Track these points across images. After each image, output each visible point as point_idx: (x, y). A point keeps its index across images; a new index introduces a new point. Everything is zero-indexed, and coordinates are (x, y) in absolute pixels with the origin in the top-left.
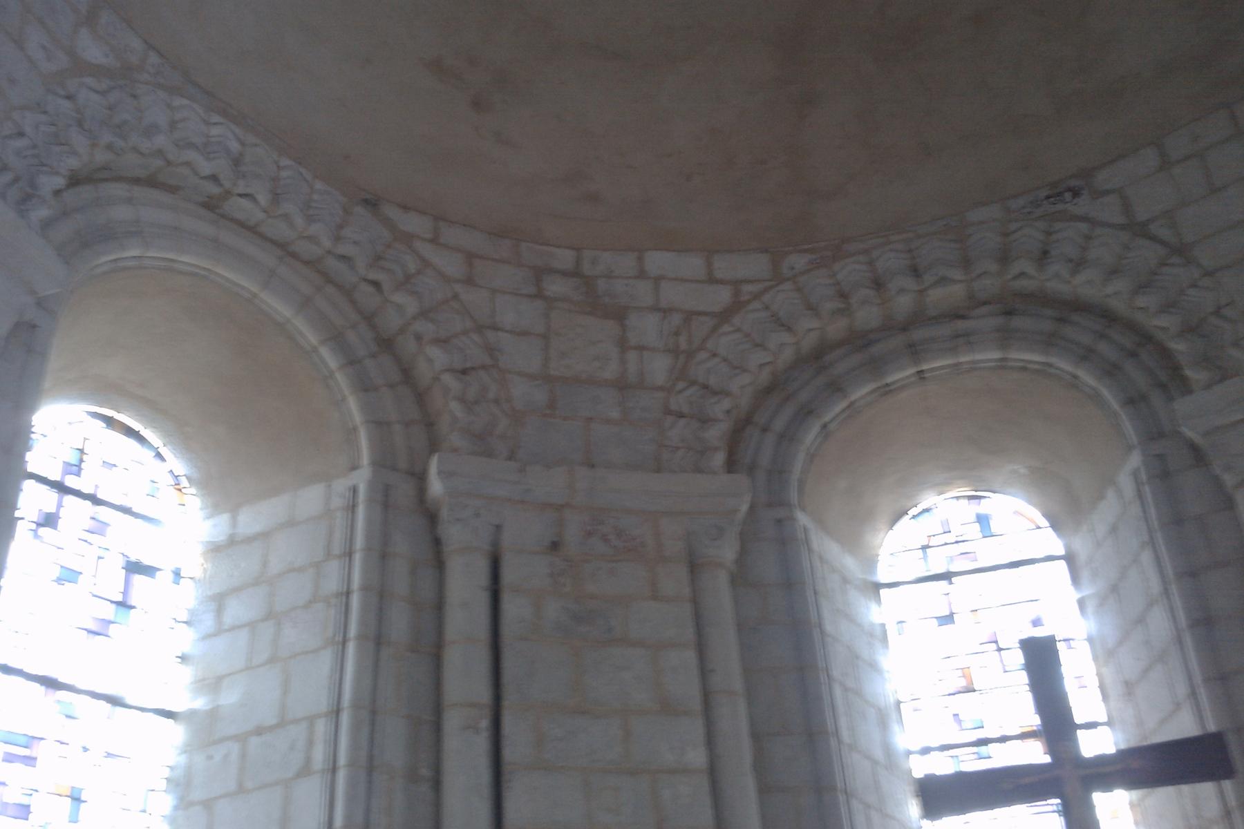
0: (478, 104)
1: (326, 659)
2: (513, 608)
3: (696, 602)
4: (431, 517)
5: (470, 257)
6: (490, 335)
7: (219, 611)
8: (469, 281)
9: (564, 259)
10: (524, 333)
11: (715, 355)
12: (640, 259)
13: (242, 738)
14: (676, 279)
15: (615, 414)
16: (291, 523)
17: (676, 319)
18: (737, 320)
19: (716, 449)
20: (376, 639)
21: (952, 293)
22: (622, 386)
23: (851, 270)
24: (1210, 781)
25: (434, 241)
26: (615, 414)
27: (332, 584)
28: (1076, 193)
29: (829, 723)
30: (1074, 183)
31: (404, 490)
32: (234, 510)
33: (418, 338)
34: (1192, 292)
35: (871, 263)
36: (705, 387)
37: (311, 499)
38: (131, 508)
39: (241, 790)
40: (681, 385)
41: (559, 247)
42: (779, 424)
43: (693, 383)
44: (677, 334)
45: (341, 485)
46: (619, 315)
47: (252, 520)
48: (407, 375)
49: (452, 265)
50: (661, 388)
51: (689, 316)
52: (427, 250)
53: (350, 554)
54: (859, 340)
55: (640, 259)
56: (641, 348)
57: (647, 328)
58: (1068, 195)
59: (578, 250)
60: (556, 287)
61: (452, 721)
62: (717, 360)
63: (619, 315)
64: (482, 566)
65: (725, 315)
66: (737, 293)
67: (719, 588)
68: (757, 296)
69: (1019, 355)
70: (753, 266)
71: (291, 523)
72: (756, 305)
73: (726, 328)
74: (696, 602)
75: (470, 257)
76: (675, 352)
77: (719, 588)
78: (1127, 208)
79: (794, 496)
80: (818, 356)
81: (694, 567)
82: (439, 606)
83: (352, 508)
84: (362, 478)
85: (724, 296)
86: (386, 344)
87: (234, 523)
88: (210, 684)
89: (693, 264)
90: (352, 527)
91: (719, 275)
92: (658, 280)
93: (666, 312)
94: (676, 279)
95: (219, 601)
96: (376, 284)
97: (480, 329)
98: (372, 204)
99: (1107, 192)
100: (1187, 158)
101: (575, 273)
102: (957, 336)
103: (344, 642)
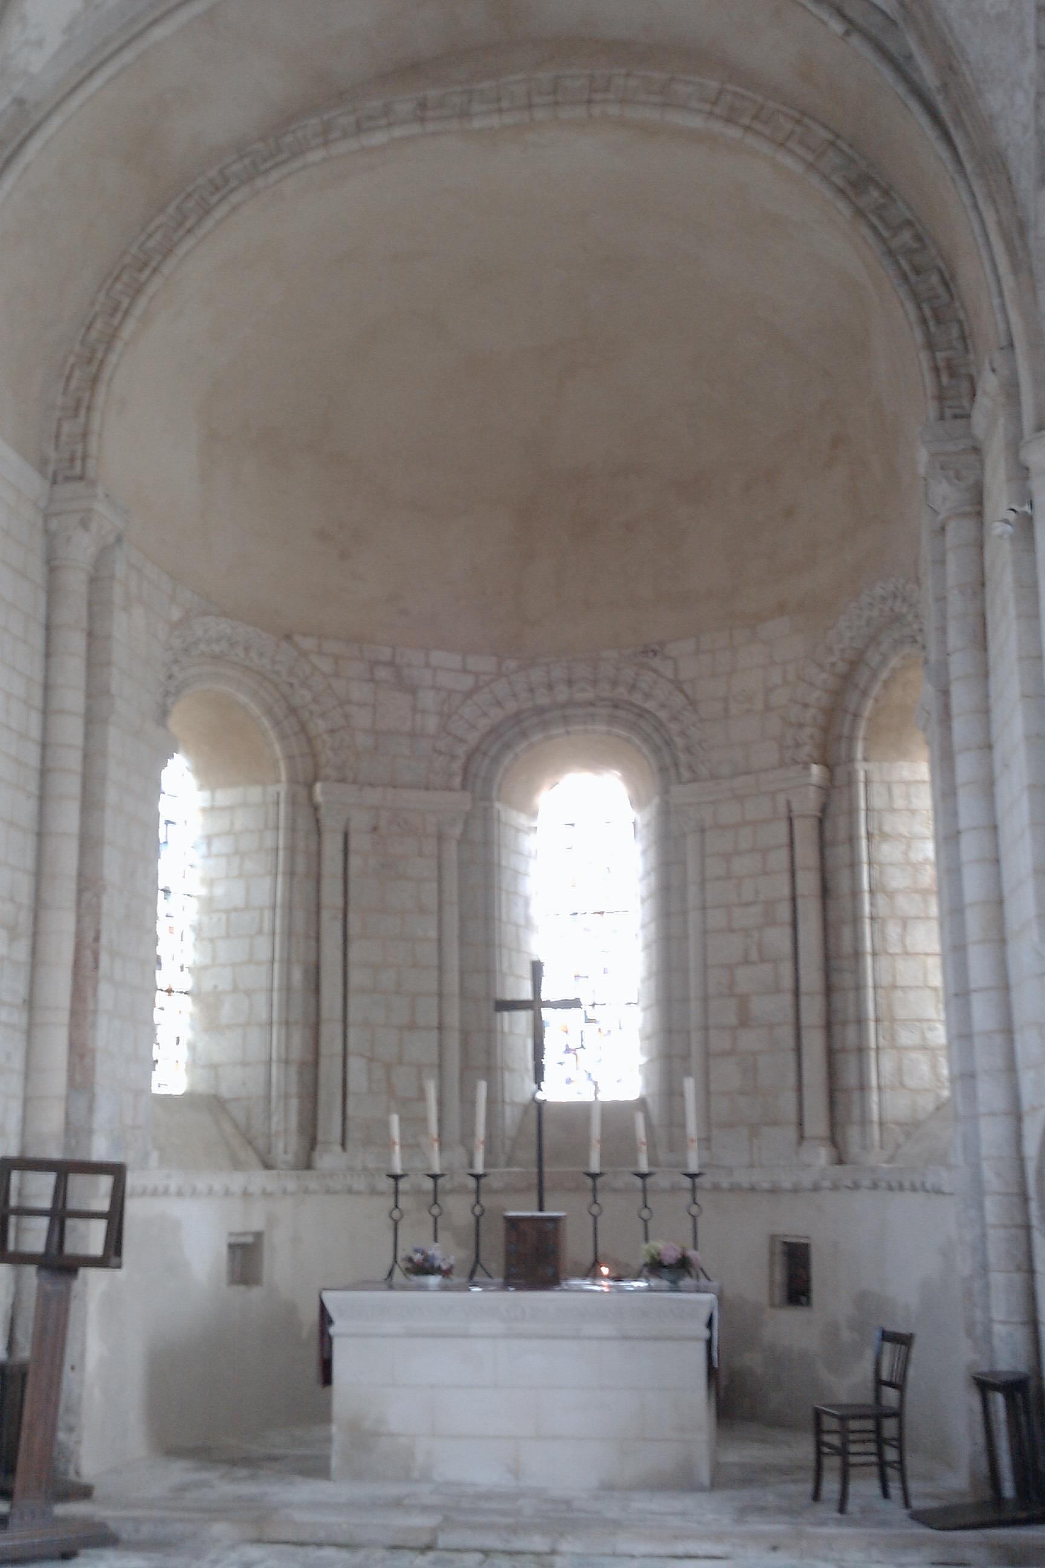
1: (267, 882)
2: (355, 862)
3: (439, 857)
4: (316, 808)
7: (209, 845)
8: (337, 675)
9: (386, 653)
13: (227, 912)
16: (245, 805)
20: (291, 874)
21: (589, 695)
23: (537, 675)
24: (5, 1263)
27: (269, 842)
28: (655, 652)
30: (657, 648)
31: (302, 793)
32: (213, 791)
33: (311, 712)
37: (255, 793)
39: (228, 936)
43: (449, 734)
45: (272, 790)
46: (413, 691)
47: (224, 797)
48: (303, 727)
49: (326, 665)
53: (277, 828)
54: (540, 711)
57: (428, 699)
60: (382, 673)
61: (326, 915)
63: (413, 691)
64: (340, 839)
65: (469, 694)
67: (452, 852)
69: (617, 730)
70: (485, 664)
71: (245, 805)
73: (469, 702)
74: (439, 857)
77: (452, 852)
78: (676, 670)
79: (494, 794)
80: (517, 717)
82: (319, 854)
84: (282, 788)
85: (468, 682)
86: (293, 711)
87: (213, 798)
88: (210, 883)
90: (278, 814)
95: (209, 839)
96: (291, 685)
98: (288, 637)
99: (670, 658)
101: (391, 664)
103: (276, 874)
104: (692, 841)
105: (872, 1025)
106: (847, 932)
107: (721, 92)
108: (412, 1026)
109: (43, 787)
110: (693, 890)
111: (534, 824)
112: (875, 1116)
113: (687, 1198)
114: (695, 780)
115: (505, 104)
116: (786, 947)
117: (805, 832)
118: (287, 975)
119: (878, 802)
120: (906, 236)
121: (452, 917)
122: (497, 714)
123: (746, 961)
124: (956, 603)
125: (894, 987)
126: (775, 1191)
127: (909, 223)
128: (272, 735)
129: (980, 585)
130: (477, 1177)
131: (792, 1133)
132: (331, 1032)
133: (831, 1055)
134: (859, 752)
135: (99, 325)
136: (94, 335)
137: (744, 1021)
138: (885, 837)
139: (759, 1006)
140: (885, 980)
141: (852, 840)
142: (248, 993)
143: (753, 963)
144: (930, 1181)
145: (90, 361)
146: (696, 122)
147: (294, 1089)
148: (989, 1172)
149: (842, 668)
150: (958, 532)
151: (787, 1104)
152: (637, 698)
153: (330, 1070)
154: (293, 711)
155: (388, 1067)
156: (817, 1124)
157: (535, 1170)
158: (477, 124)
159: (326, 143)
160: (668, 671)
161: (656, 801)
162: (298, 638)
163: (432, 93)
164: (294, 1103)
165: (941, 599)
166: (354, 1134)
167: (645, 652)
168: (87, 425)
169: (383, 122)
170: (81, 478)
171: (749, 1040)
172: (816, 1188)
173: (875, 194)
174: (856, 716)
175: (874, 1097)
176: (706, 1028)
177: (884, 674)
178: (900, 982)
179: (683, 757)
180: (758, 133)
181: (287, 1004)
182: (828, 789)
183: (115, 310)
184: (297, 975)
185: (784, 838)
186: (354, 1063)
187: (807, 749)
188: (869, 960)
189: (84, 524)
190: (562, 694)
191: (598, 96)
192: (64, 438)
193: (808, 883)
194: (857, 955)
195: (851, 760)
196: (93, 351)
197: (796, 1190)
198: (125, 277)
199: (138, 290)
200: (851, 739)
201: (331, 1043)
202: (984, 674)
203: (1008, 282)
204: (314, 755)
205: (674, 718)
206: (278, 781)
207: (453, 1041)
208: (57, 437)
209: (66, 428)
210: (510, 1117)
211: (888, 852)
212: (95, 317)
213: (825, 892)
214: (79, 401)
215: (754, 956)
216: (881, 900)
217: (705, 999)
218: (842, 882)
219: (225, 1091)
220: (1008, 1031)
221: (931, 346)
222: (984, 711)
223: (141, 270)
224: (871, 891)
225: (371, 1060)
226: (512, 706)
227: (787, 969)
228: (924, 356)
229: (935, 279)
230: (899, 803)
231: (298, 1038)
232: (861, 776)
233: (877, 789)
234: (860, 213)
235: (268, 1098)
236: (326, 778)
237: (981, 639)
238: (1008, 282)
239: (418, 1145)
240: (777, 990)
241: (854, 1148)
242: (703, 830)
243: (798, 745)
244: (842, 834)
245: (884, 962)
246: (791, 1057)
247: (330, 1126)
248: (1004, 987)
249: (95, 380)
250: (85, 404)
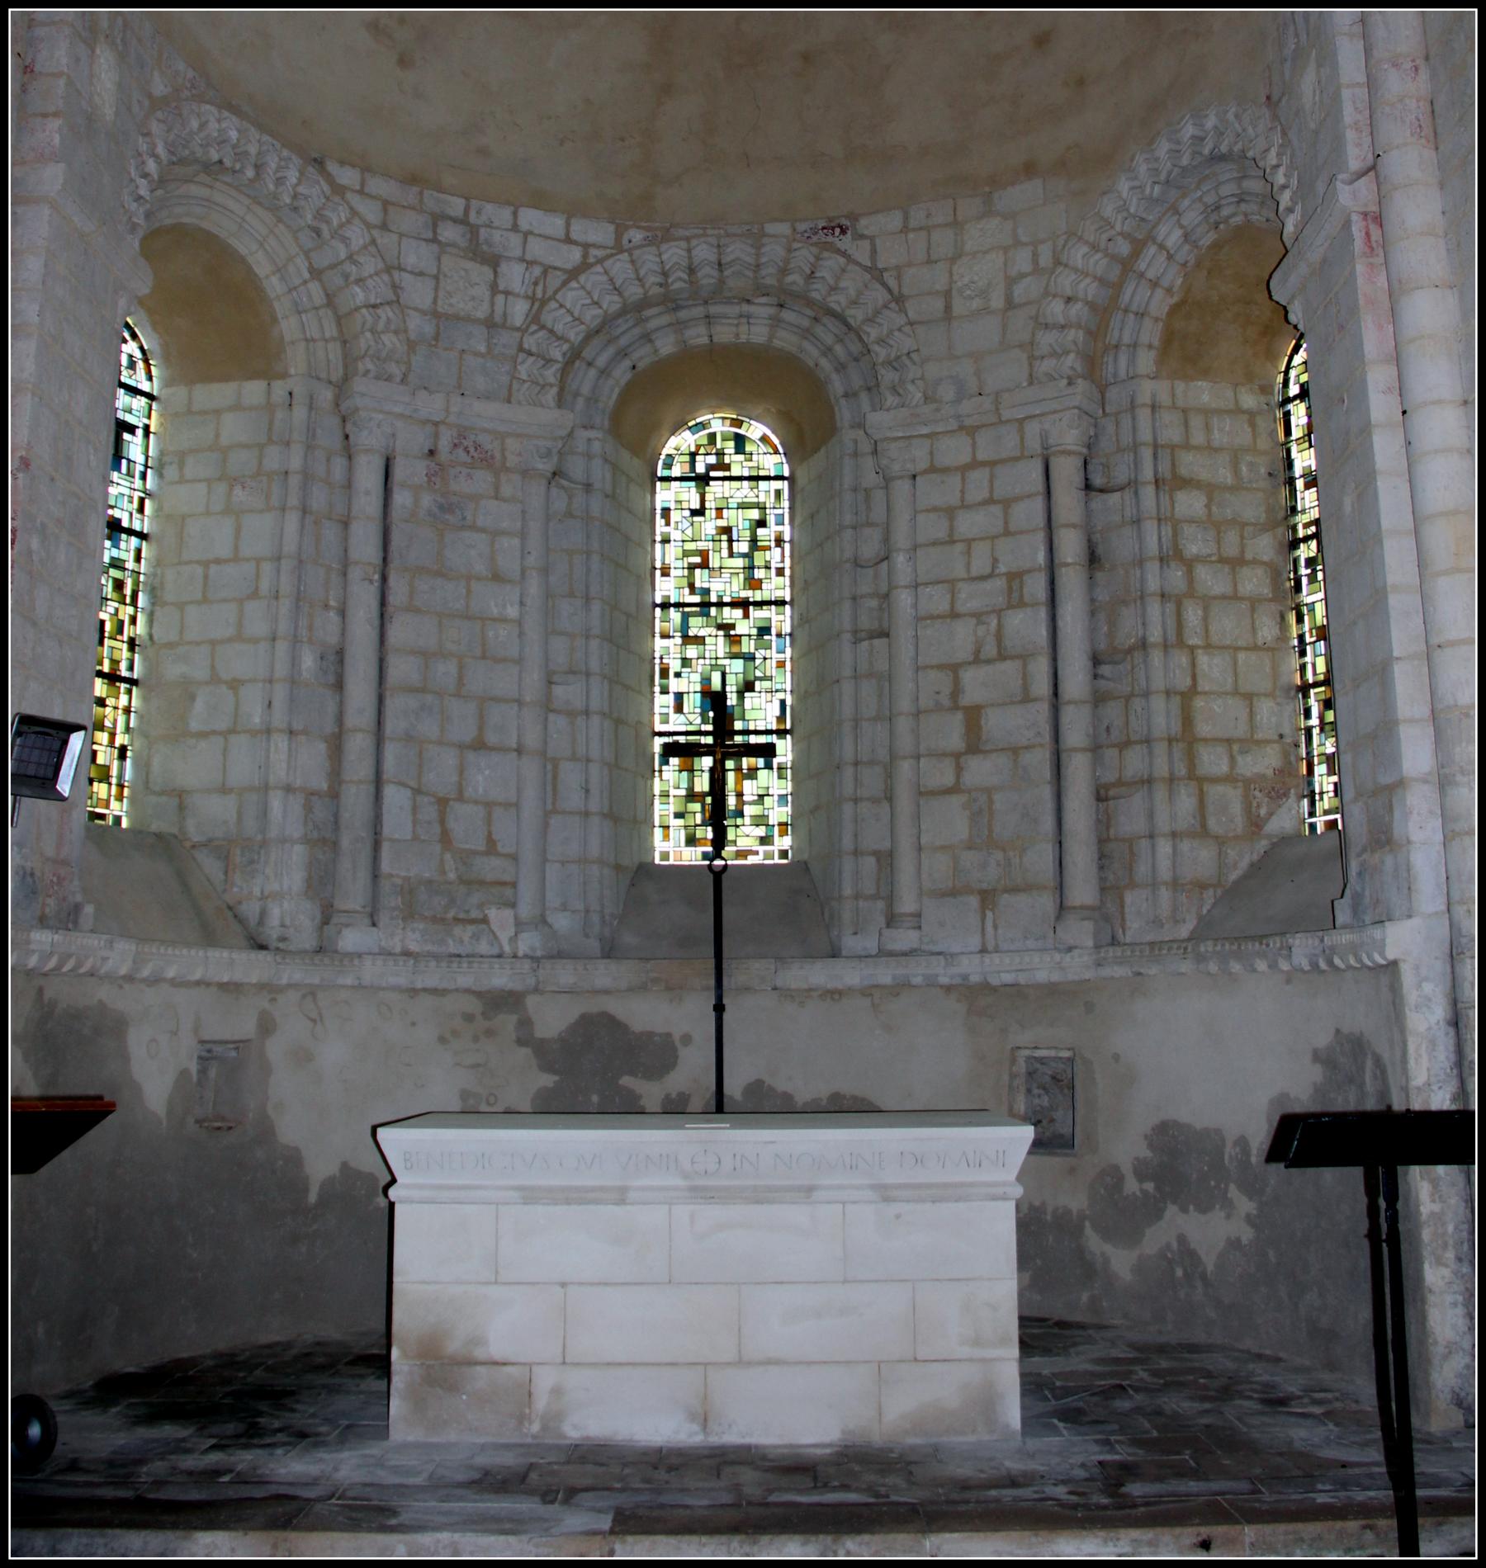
0: (404, 62)
2: (401, 498)
5: (386, 204)
6: (396, 274)
8: (384, 227)
9: (456, 206)
10: (421, 274)
11: (561, 306)
12: (515, 214)
14: (540, 235)
15: (482, 349)
17: (537, 271)
18: (582, 278)
19: (551, 385)
22: (490, 324)
25: (361, 192)
26: (482, 349)
28: (843, 231)
29: (614, 397)
30: (844, 222)
34: (896, 333)
35: (689, 251)
36: (551, 331)
38: (1366, 1236)
40: (534, 327)
41: (453, 195)
42: (601, 361)
43: (543, 327)
44: (536, 284)
46: (494, 262)
49: (370, 211)
50: (518, 329)
51: (547, 270)
52: (355, 200)
55: (515, 214)
56: (507, 293)
57: (514, 276)
58: (838, 231)
59: (467, 199)
60: (449, 232)
62: (563, 311)
63: (494, 262)
64: (378, 464)
65: (574, 274)
66: (585, 256)
68: (600, 261)
70: (599, 233)
72: (599, 268)
73: (574, 284)
75: (386, 204)
76: (532, 299)
78: (874, 252)
85: (576, 255)
89: (554, 224)
91: (574, 236)
92: (527, 234)
93: (530, 264)
94: (540, 235)
97: (388, 269)
98: (319, 163)
100: (921, 229)
101: (463, 221)
102: (741, 316)
123: (977, 660)
137: (975, 743)
139: (999, 724)
143: (989, 662)
151: (1041, 859)
153: (355, 800)
155: (442, 803)
160: (861, 253)
162: (332, 167)
166: (389, 901)
167: (829, 229)
171: (980, 771)
201: (358, 765)
215: (990, 650)
225: (417, 791)
227: (1040, 668)
239: (485, 920)
240: (1027, 698)
247: (353, 893)
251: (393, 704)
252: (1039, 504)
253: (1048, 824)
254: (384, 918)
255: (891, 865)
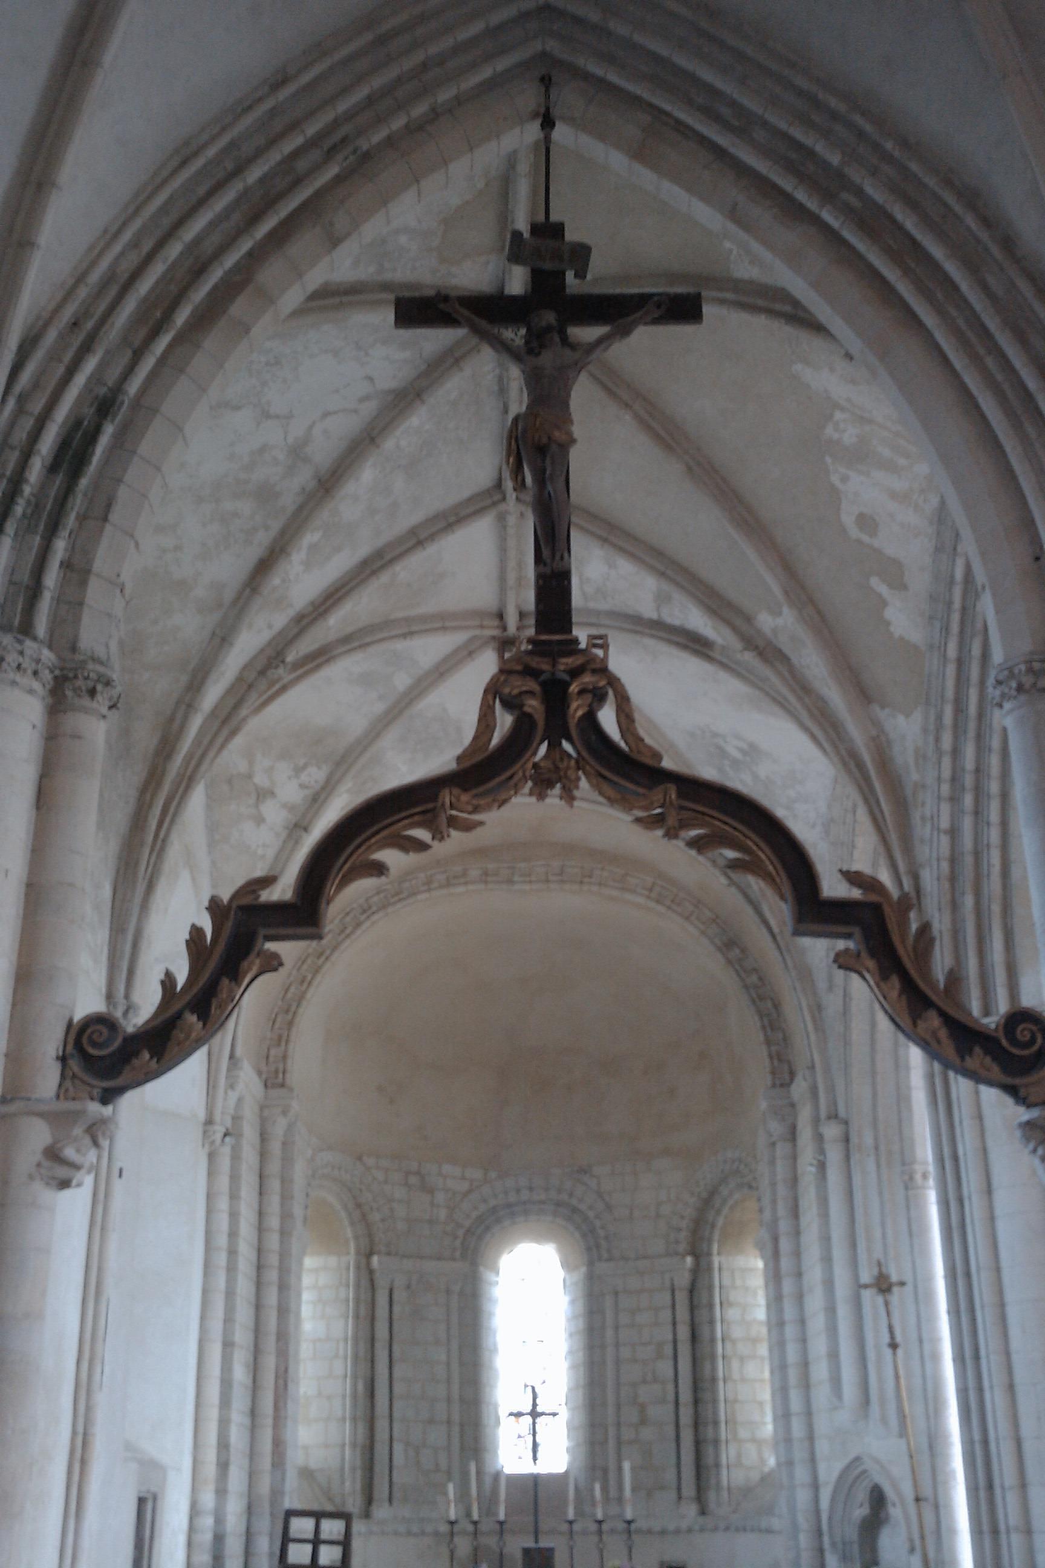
2: (397, 1309)
8: (386, 1182)
20: (357, 1317)
21: (543, 1197)
28: (586, 1173)
31: (364, 1261)
37: (332, 1261)
46: (431, 1191)
48: (364, 1216)
49: (380, 1175)
53: (348, 1286)
54: (509, 1206)
57: (440, 1197)
63: (431, 1191)
64: (387, 1292)
70: (477, 1174)
80: (494, 1210)
81: (448, 1292)
83: (348, 1269)
84: (351, 1258)
85: (466, 1186)
86: (359, 1206)
98: (360, 1158)
101: (418, 1173)
103: (348, 1317)
104: (609, 1301)
105: (723, 1426)
106: (707, 1366)
107: (654, 884)
108: (431, 1421)
109: (259, 1276)
110: (609, 1333)
111: (497, 1279)
112: (725, 1483)
113: (596, 1539)
114: (609, 1260)
115: (533, 878)
116: (670, 1373)
117: (682, 1298)
118: (354, 1386)
119: (726, 1282)
120: (754, 978)
121: (455, 1346)
122: (483, 1208)
124: (782, 1191)
125: (736, 1401)
126: (663, 1532)
127: (755, 970)
128: (346, 1223)
129: (794, 1181)
130: (475, 1523)
131: (673, 1495)
132: (382, 1425)
133: (698, 1444)
134: (715, 1247)
135: (292, 989)
136: (289, 995)
137: (643, 1421)
138: (730, 1305)
139: (653, 1412)
140: (730, 1396)
141: (711, 1306)
142: (329, 1398)
144: (764, 1525)
145: (287, 1011)
146: (641, 900)
147: (358, 1463)
148: (801, 1519)
149: (705, 1195)
150: (782, 1149)
151: (670, 1475)
152: (574, 1202)
153: (381, 1450)
154: (359, 1206)
156: (689, 1489)
157: (532, 1518)
158: (517, 887)
159: (429, 890)
161: (584, 1269)
162: (365, 1158)
163: (491, 866)
164: (359, 1473)
165: (773, 1185)
166: (397, 1494)
168: (286, 1051)
169: (462, 880)
170: (283, 1085)
171: (647, 1433)
172: (690, 1530)
173: (737, 951)
174: (713, 1226)
175: (724, 1472)
176: (618, 1425)
177: (731, 1202)
178: (740, 1397)
179: (603, 1243)
180: (674, 911)
181: (354, 1405)
182: (696, 1271)
183: (303, 982)
184: (361, 1387)
185: (669, 1303)
186: (398, 1448)
187: (682, 1247)
188: (721, 1384)
189: (285, 1113)
190: (525, 1195)
191: (586, 880)
192: (271, 1059)
193: (684, 1332)
194: (714, 1380)
195: (709, 1254)
196: (290, 1006)
197: (677, 1532)
198: (309, 961)
199: (317, 971)
200: (710, 1241)
201: (382, 1435)
202: (797, 1233)
203: (813, 1037)
204: (370, 1236)
205: (597, 1217)
206: (348, 1253)
207: (456, 1429)
208: (267, 1057)
209: (273, 1052)
210: (488, 1481)
211: (732, 1314)
212: (290, 985)
213: (694, 1338)
214: (280, 1037)
216: (728, 1345)
217: (618, 1407)
218: (705, 1331)
219: (313, 1464)
220: (811, 1438)
221: (768, 1042)
222: (797, 1254)
223: (319, 957)
224: (723, 1340)
226: (493, 1202)
227: (670, 1387)
228: (764, 1048)
229: (769, 1004)
230: (738, 1282)
231: (361, 1430)
232: (716, 1265)
233: (726, 1274)
234: (729, 962)
235: (342, 1469)
236: (379, 1253)
237: (795, 1213)
238: (813, 1037)
241: (712, 1505)
242: (616, 1293)
243: (677, 1242)
244: (704, 1301)
245: (730, 1385)
246: (673, 1445)
248: (809, 1414)
249: (290, 1024)
250: (284, 1038)
251: (397, 1405)
252: (669, 1313)
253: (673, 1461)
254: (395, 1502)
255: (710, 1277)
